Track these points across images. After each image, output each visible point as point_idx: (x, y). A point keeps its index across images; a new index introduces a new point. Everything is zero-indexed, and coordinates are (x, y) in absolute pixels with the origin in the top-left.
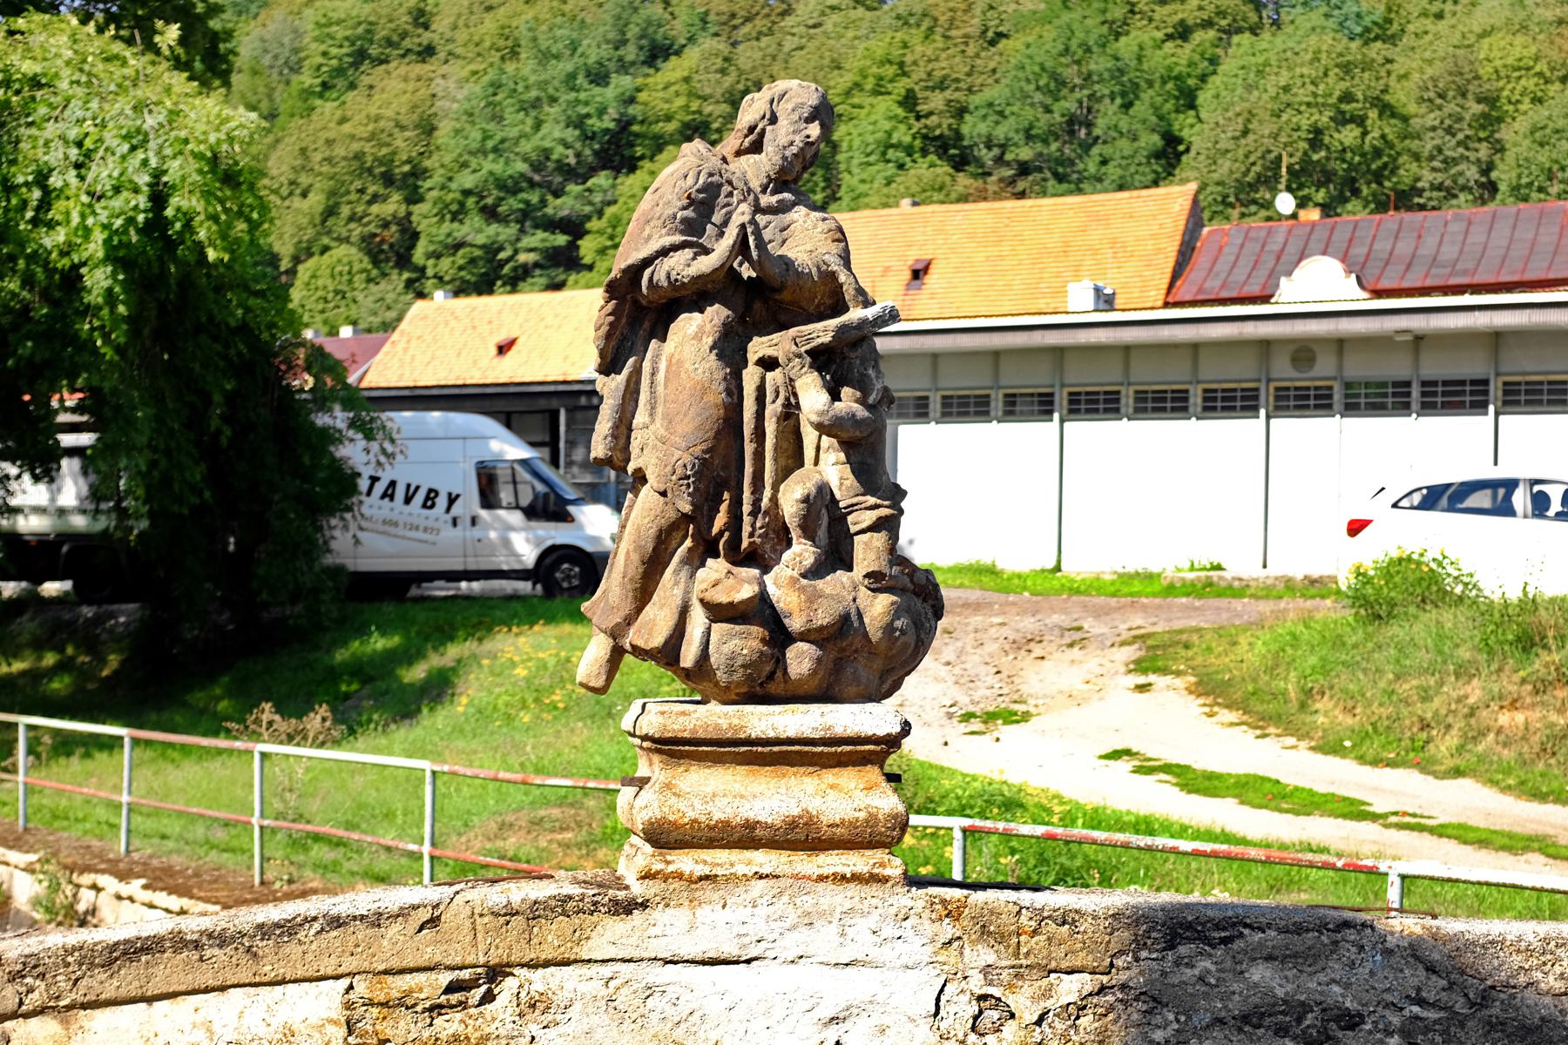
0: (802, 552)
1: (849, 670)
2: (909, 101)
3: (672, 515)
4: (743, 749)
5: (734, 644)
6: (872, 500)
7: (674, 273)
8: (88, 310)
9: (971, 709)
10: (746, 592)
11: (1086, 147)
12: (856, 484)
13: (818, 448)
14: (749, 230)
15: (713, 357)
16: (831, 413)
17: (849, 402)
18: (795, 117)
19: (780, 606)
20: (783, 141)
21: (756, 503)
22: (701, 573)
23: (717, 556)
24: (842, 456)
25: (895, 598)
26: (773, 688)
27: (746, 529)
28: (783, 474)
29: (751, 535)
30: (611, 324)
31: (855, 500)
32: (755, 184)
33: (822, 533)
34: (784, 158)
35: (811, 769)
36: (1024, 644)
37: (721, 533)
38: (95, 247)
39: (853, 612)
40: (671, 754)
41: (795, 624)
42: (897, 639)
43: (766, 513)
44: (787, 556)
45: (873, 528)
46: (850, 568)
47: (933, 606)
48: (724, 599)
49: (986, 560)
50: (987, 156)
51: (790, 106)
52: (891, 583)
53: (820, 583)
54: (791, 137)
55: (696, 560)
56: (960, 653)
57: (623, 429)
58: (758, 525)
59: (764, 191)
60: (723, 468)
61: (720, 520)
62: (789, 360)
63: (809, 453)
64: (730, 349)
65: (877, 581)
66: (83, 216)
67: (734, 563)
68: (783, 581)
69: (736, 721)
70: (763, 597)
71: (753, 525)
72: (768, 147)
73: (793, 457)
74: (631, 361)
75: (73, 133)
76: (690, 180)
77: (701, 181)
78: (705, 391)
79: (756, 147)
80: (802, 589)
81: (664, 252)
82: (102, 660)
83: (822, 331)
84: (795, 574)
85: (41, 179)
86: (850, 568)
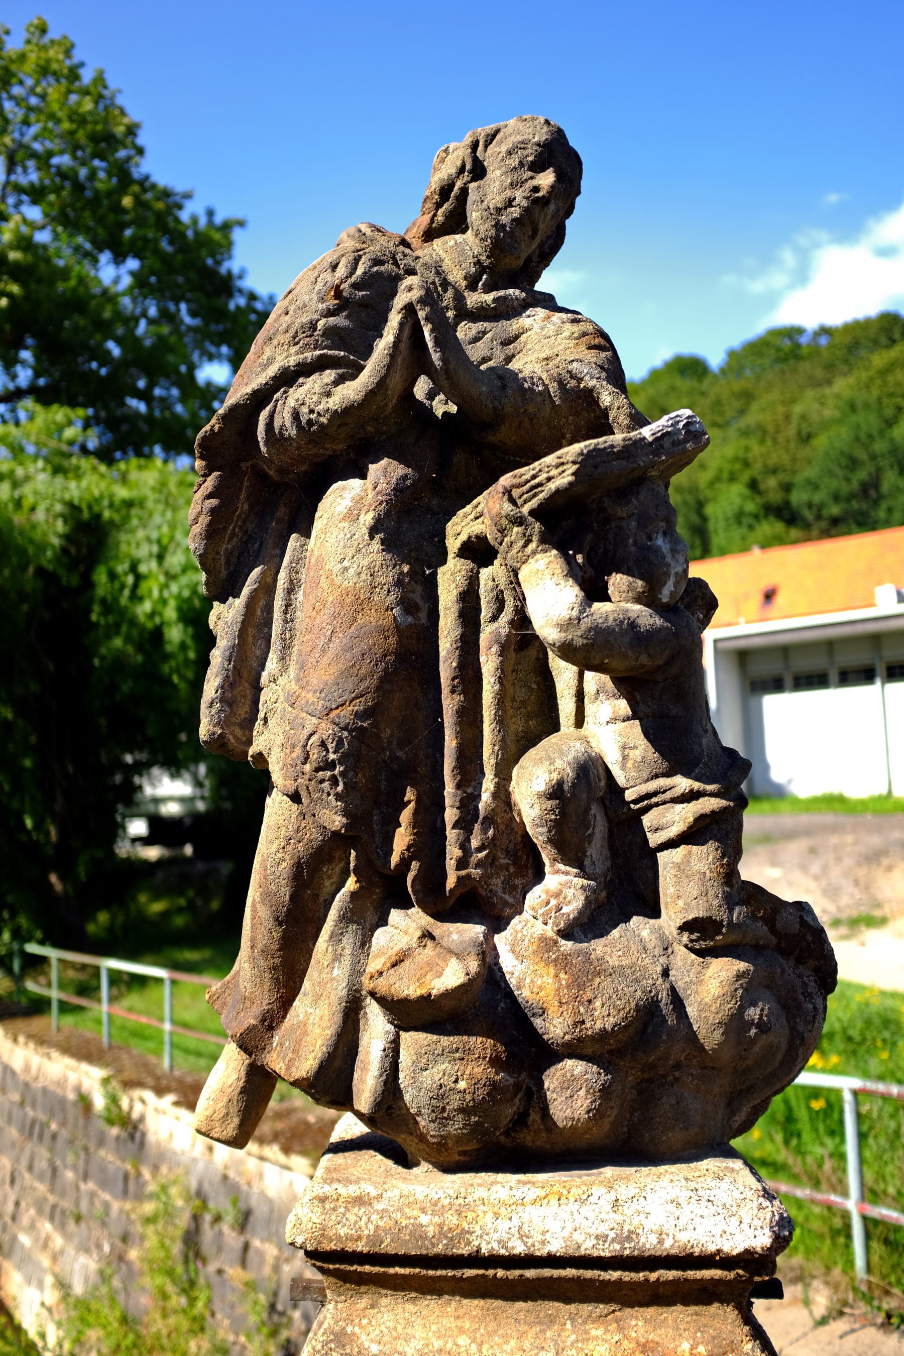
0: (561, 888)
1: (667, 1102)
2: (753, 485)
3: (314, 836)
4: (470, 1273)
5: (439, 1073)
6: (682, 784)
7: (305, 410)
8: (167, 657)
9: (839, 916)
10: (452, 976)
11: (876, 503)
12: (652, 754)
13: (580, 696)
14: (421, 314)
15: (376, 545)
16: (586, 623)
17: (622, 602)
18: (514, 161)
19: (524, 994)
20: (495, 199)
21: (468, 803)
22: (380, 936)
23: (405, 904)
24: (623, 707)
25: (742, 966)
26: (527, 1138)
27: (453, 852)
28: (515, 748)
29: (462, 864)
30: (213, 512)
31: (652, 786)
32: (457, 276)
33: (596, 850)
34: (498, 226)
35: (602, 1308)
36: (873, 858)
37: (405, 864)
38: (170, 613)
39: (664, 996)
40: (344, 1278)
41: (555, 1027)
42: (753, 1041)
43: (489, 821)
44: (535, 896)
45: (692, 836)
46: (654, 912)
47: (816, 970)
48: (412, 991)
49: (836, 791)
50: (809, 515)
51: (504, 149)
52: (733, 938)
53: (598, 947)
54: (509, 193)
55: (368, 915)
56: (825, 869)
57: (245, 687)
58: (475, 843)
59: (472, 285)
60: (401, 744)
61: (402, 839)
62: (502, 531)
63: (566, 706)
64: (410, 533)
65: (705, 936)
66: (161, 591)
67: (441, 916)
68: (529, 946)
69: (452, 1220)
70: (491, 977)
71: (464, 845)
72: (474, 215)
73: (535, 715)
74: (256, 572)
75: (154, 535)
76: (341, 271)
77: (359, 271)
78: (360, 605)
79: (457, 222)
80: (563, 962)
81: (287, 378)
82: (208, 901)
83: (557, 469)
84: (550, 931)
85: (134, 568)
86: (654, 912)
